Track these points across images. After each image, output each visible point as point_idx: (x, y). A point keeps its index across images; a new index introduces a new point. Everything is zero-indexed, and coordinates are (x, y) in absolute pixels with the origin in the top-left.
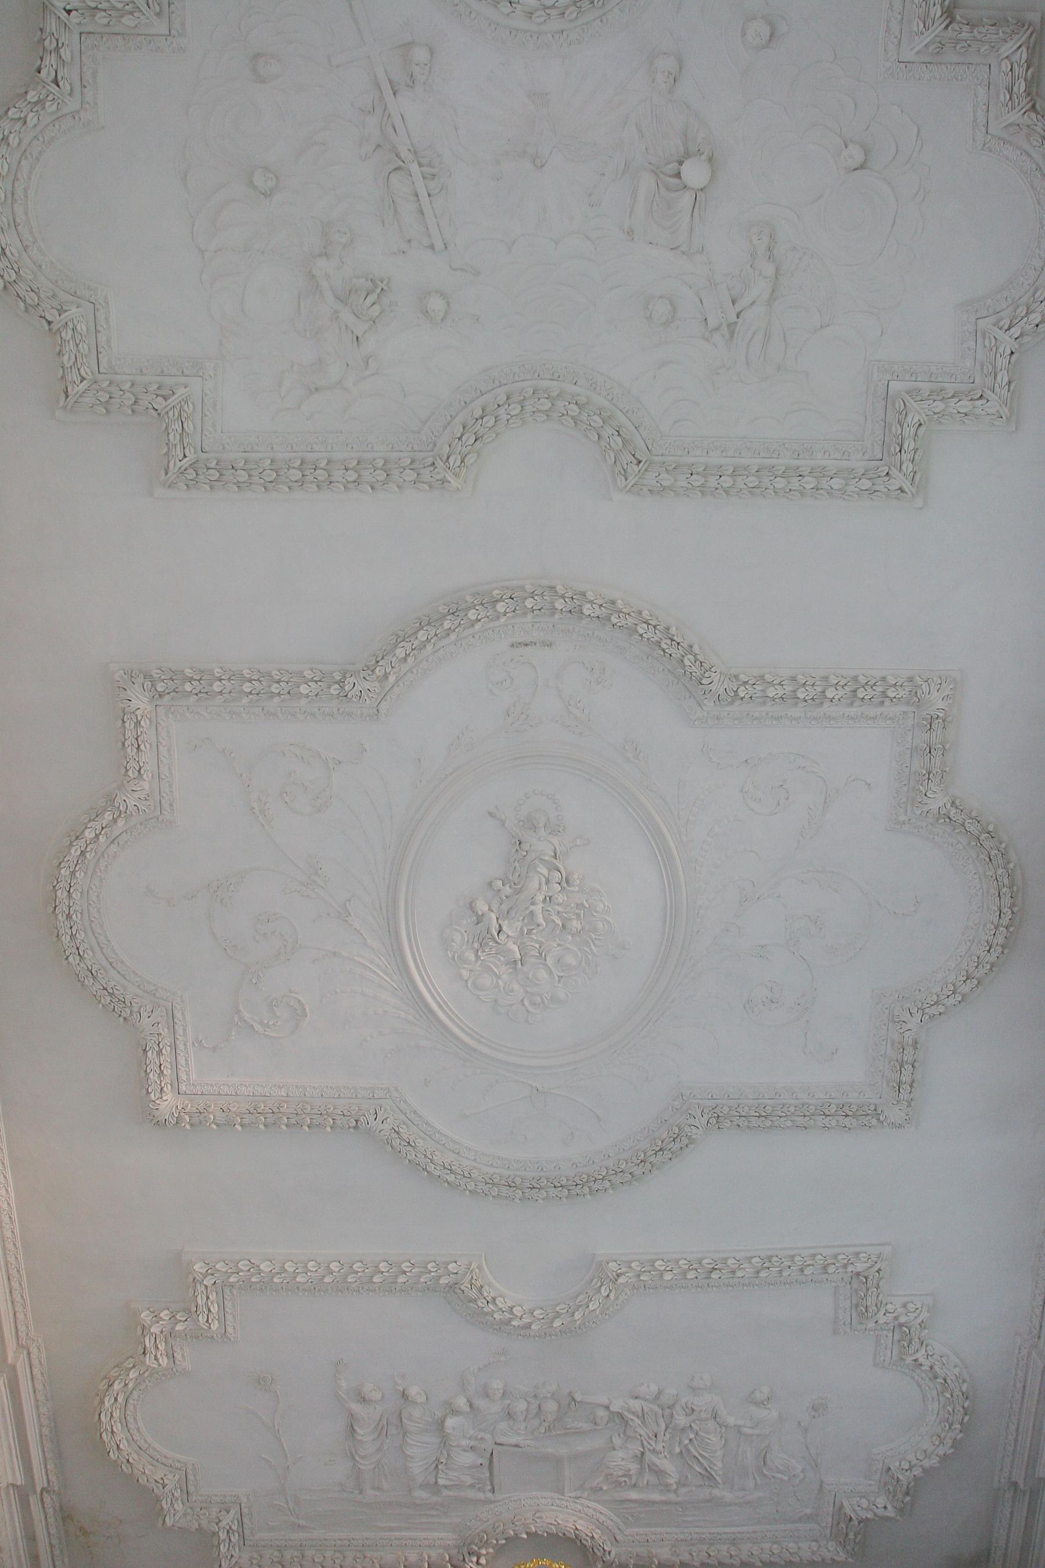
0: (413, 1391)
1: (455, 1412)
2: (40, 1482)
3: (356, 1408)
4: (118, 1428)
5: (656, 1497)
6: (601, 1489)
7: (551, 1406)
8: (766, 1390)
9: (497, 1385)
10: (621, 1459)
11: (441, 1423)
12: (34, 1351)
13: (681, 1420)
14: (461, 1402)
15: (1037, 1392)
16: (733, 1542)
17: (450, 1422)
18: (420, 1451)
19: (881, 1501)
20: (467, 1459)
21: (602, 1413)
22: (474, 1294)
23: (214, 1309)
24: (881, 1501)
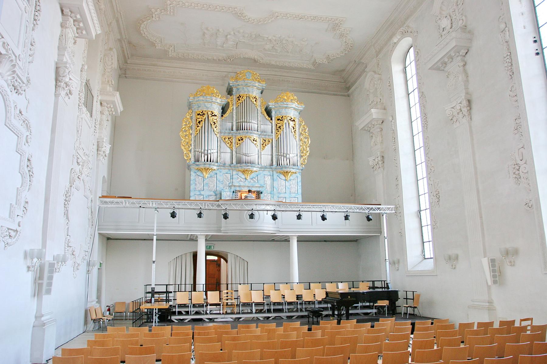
0: (221, 30)
1: (230, 34)
2: (124, 37)
3: (206, 31)
4: (144, 30)
5: (274, 53)
6: (412, 333)
7: (254, 36)
8: (306, 39)
9: (242, 31)
10: (268, 47)
11: (227, 36)
12: (122, 13)
13: (284, 42)
14: (232, 33)
15: (367, 77)
16: (289, 63)
17: (229, 36)
18: (220, 41)
19: (325, 60)
20: (232, 43)
21: (266, 39)
22: (240, 15)
23: (172, 10)
24: (325, 60)
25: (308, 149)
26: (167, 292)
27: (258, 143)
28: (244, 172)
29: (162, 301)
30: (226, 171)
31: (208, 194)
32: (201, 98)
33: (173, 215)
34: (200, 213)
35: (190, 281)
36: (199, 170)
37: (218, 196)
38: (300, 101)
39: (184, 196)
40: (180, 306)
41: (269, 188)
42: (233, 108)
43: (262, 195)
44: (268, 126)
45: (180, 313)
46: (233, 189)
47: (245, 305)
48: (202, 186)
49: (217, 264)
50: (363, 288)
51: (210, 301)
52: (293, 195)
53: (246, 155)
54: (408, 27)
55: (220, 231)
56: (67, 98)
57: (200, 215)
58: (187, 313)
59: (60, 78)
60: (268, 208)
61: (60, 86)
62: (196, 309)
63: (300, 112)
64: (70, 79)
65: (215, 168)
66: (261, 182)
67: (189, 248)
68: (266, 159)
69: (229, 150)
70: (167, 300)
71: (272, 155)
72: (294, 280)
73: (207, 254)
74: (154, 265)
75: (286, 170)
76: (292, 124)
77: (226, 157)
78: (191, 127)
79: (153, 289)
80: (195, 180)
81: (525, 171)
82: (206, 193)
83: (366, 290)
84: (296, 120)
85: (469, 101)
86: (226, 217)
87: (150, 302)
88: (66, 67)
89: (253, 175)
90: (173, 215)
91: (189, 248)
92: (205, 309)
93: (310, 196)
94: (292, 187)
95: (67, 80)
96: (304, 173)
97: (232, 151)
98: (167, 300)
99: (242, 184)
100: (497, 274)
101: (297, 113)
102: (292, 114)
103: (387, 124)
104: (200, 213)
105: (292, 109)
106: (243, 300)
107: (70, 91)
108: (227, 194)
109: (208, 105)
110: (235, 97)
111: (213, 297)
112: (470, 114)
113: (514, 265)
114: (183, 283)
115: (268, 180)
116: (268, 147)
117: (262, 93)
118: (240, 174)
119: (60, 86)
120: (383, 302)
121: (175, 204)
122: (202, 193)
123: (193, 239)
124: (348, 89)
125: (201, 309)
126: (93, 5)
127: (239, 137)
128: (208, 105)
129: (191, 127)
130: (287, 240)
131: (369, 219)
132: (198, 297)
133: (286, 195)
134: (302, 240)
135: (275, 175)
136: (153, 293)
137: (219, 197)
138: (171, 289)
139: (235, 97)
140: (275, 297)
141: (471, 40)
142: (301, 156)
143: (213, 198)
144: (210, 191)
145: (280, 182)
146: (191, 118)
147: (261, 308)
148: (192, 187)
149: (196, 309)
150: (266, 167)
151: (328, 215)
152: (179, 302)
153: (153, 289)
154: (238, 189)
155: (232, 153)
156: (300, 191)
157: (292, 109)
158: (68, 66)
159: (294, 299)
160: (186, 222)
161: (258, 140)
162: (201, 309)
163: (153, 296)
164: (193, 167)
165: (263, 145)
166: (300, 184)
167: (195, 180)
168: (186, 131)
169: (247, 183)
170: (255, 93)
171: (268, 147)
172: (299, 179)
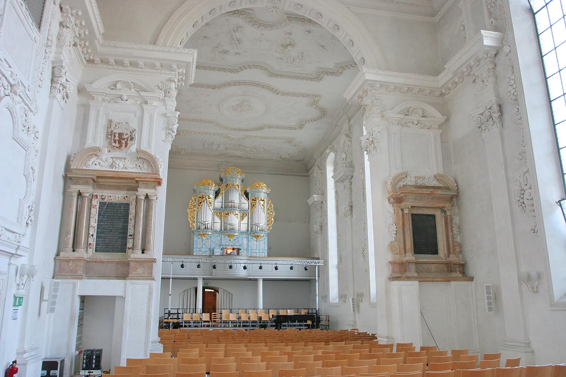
10: (247, 149)
18: (214, 147)
25: (273, 219)
26: (178, 313)
27: (239, 216)
28: (229, 236)
29: (174, 319)
30: (217, 235)
31: (205, 251)
32: (202, 187)
33: (182, 266)
34: (199, 265)
35: (192, 307)
36: (199, 235)
37: (212, 252)
38: (268, 187)
39: (189, 252)
40: (186, 322)
41: (245, 247)
42: (223, 191)
43: (240, 251)
44: (246, 204)
45: (185, 326)
46: (221, 247)
47: (225, 322)
48: (201, 246)
49: (214, 295)
50: (303, 312)
51: (204, 319)
52: (261, 251)
53: (230, 224)
54: (333, 146)
55: (212, 275)
56: (63, 102)
57: (198, 266)
58: (190, 326)
59: (55, 79)
60: (241, 261)
61: (55, 88)
62: (195, 324)
63: (268, 194)
64: (67, 81)
65: (210, 233)
66: (241, 242)
67: (192, 285)
68: (244, 228)
69: (220, 221)
70: (178, 318)
71: (248, 224)
72: (259, 306)
73: (204, 288)
74: (170, 297)
75: (256, 234)
76: (262, 202)
77: (218, 226)
78: (195, 206)
79: (169, 311)
80: (197, 241)
81: (530, 198)
82: (204, 250)
83: (304, 314)
84: (265, 200)
85: (352, 206)
86: (214, 267)
87: (168, 318)
88: (62, 66)
89: (235, 237)
90: (182, 266)
91: (192, 285)
92: (200, 324)
93: (272, 252)
94: (261, 246)
95: (64, 81)
96: (269, 235)
97: (221, 221)
98: (178, 318)
99: (227, 243)
100: (492, 301)
101: (266, 195)
102: (263, 196)
103: (323, 203)
104: (199, 265)
105: (263, 192)
106: (224, 319)
107: (67, 93)
108: (218, 252)
109: (207, 191)
110: (224, 185)
111: (206, 317)
112: (352, 214)
113: (537, 292)
114: (188, 308)
115: (245, 241)
116: (246, 218)
117: (242, 181)
118: (227, 237)
119: (55, 88)
120: (312, 320)
121: (183, 259)
122: (201, 249)
123: (196, 279)
124: (308, 171)
125: (198, 324)
126: (96, 5)
127: (226, 212)
128: (207, 191)
129: (195, 206)
130: (256, 280)
131: (306, 269)
132: (196, 317)
133: (257, 251)
134: (264, 280)
135: (250, 237)
136: (169, 314)
137: (212, 254)
138: (180, 311)
139: (224, 185)
140: (244, 318)
141: (353, 171)
142: (268, 225)
143: (208, 254)
144: (207, 248)
145: (254, 243)
146: (195, 200)
147: (235, 324)
148: (195, 246)
149: (195, 324)
150: (243, 233)
151: (279, 266)
152: (185, 319)
153: (169, 311)
154: (225, 247)
155: (221, 223)
156: (266, 248)
157: (263, 192)
158: (64, 65)
159: (256, 319)
160: (190, 270)
161: (239, 214)
162: (198, 324)
163: (169, 316)
164: (196, 233)
165: (242, 218)
166: (266, 243)
167: (197, 241)
168: (191, 208)
169: (231, 243)
170: (238, 182)
171: (246, 218)
172: (266, 240)
